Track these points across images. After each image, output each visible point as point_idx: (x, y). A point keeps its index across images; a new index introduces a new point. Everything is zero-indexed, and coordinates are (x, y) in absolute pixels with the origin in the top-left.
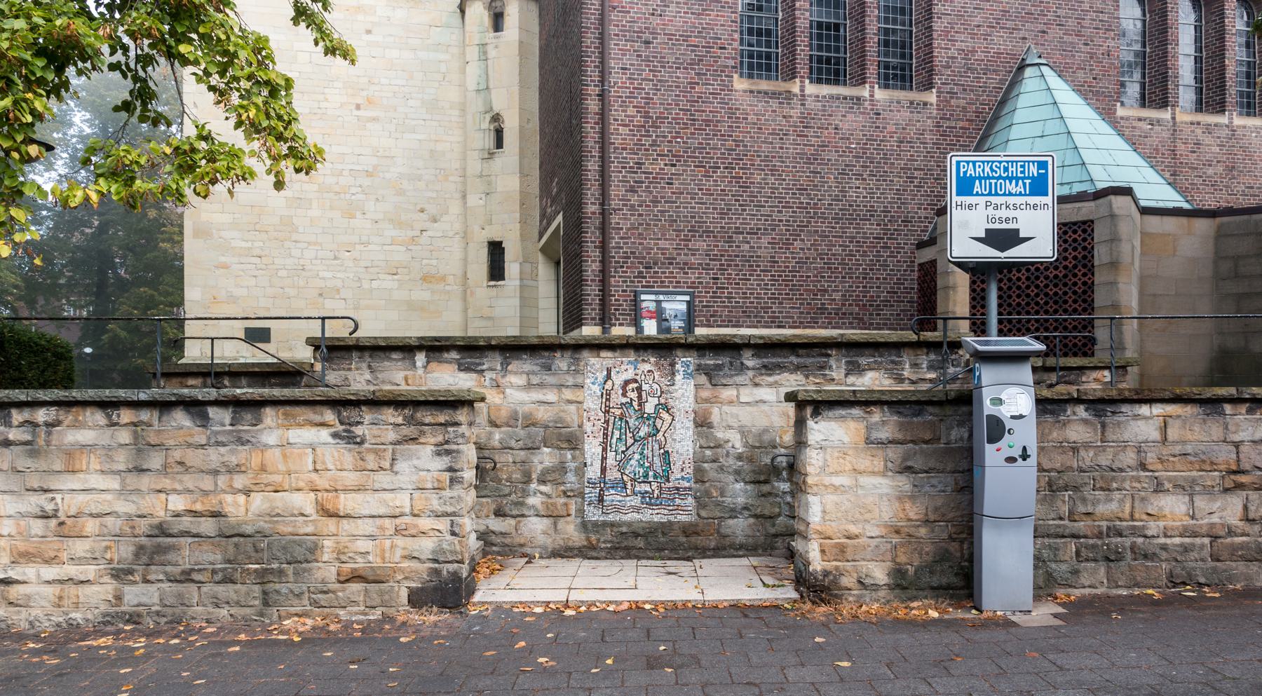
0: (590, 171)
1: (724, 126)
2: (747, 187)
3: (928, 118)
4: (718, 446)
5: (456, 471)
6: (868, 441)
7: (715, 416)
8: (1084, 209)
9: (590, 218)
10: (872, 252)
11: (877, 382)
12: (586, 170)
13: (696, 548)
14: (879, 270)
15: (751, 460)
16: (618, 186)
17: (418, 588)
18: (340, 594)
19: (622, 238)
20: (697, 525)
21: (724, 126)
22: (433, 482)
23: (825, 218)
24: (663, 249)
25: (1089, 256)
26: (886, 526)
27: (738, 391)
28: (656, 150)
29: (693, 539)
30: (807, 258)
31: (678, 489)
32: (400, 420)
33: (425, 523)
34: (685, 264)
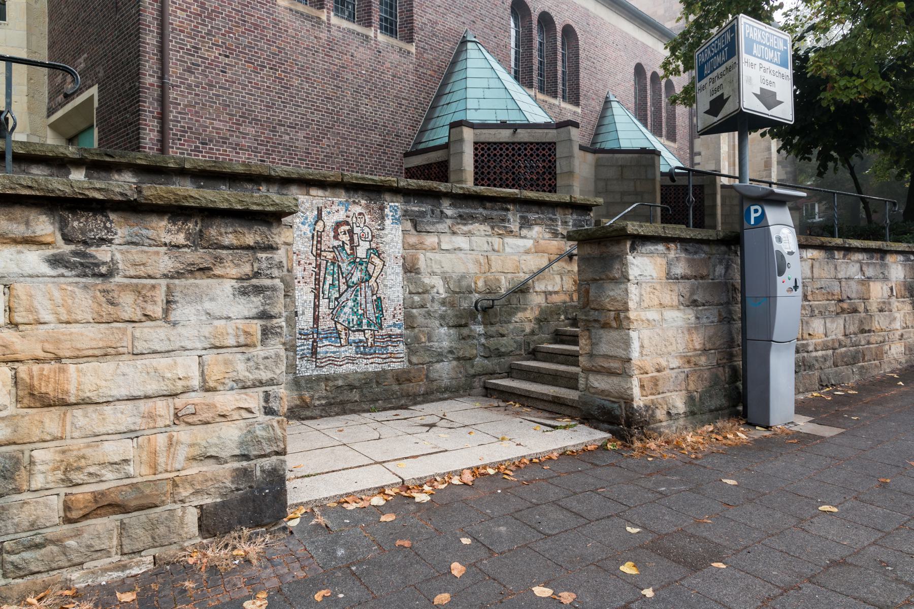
0: (148, 44)
1: (269, 33)
2: (288, 88)
3: (411, 63)
4: (426, 292)
5: (271, 317)
6: (669, 276)
7: (422, 264)
8: (550, 134)
9: (148, 89)
10: (376, 155)
11: (541, 236)
12: (144, 43)
13: (408, 395)
14: (380, 169)
15: (452, 305)
16: (176, 64)
17: (216, 505)
18: (72, 543)
19: (179, 113)
20: (409, 372)
21: (269, 33)
22: (237, 336)
23: (345, 124)
24: (217, 129)
25: (553, 166)
26: (682, 357)
27: (439, 238)
28: (211, 40)
29: (405, 386)
30: (332, 154)
31: (390, 336)
32: (181, 238)
33: (226, 400)
34: (237, 145)
